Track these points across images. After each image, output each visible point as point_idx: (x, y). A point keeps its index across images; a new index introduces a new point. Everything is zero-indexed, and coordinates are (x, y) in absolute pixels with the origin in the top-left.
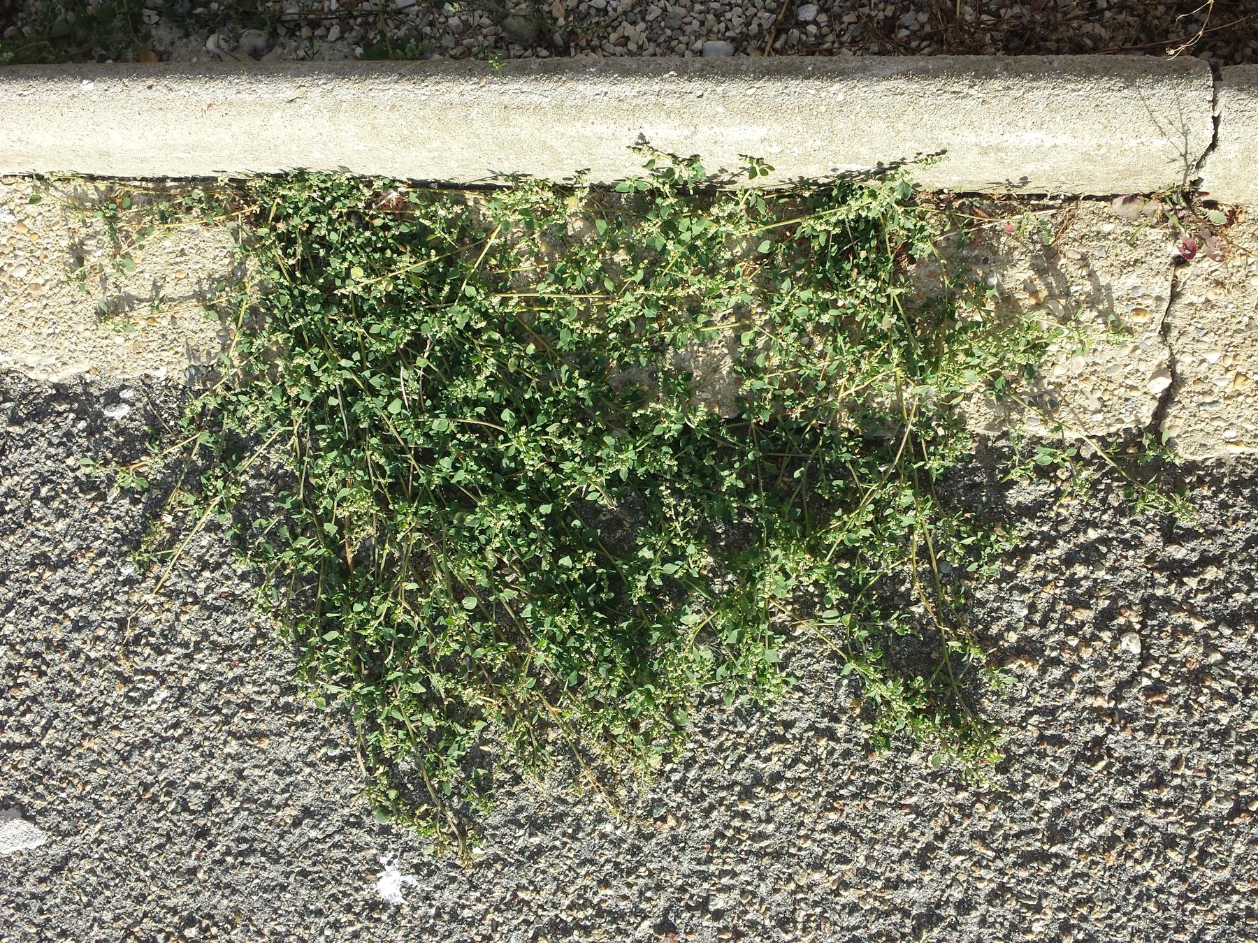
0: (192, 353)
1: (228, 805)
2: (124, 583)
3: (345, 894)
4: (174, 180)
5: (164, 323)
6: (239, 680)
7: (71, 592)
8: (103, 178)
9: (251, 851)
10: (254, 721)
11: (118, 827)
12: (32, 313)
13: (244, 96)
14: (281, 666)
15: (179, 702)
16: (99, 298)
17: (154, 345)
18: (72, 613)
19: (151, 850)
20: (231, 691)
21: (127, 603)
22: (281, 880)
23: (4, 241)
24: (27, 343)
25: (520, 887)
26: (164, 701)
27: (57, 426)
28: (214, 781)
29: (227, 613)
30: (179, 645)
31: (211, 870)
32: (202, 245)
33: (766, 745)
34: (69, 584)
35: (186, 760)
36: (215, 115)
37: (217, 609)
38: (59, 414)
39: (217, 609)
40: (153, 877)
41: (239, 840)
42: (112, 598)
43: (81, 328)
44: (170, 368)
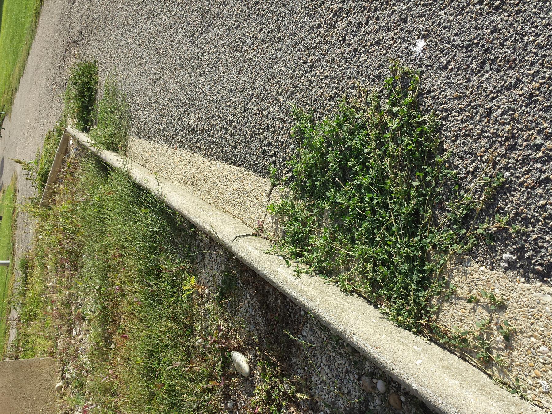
0: (465, 273)
1: (474, 66)
2: (510, 168)
3: (435, 38)
4: (456, 355)
5: (474, 291)
6: (463, 122)
7: (539, 166)
8: (487, 374)
9: (467, 47)
10: (459, 104)
11: (527, 44)
12: (541, 324)
13: (366, 345)
14: (447, 128)
15: (490, 112)
16: (503, 317)
17: (481, 282)
18: (540, 154)
19: (511, 37)
20: (467, 116)
21: (509, 158)
22: (456, 38)
23: (550, 372)
24: (547, 308)
25: (386, 54)
26: (497, 110)
27: (542, 257)
28: (479, 75)
29: (465, 151)
30: (487, 137)
31: (484, 35)
32: (452, 320)
33: (330, 109)
34: (540, 170)
35: (490, 83)
36: (378, 344)
37: (470, 154)
38: (541, 265)
39: (470, 154)
40: (512, 24)
41: (471, 51)
42: (517, 161)
43: (515, 304)
44: (478, 270)
